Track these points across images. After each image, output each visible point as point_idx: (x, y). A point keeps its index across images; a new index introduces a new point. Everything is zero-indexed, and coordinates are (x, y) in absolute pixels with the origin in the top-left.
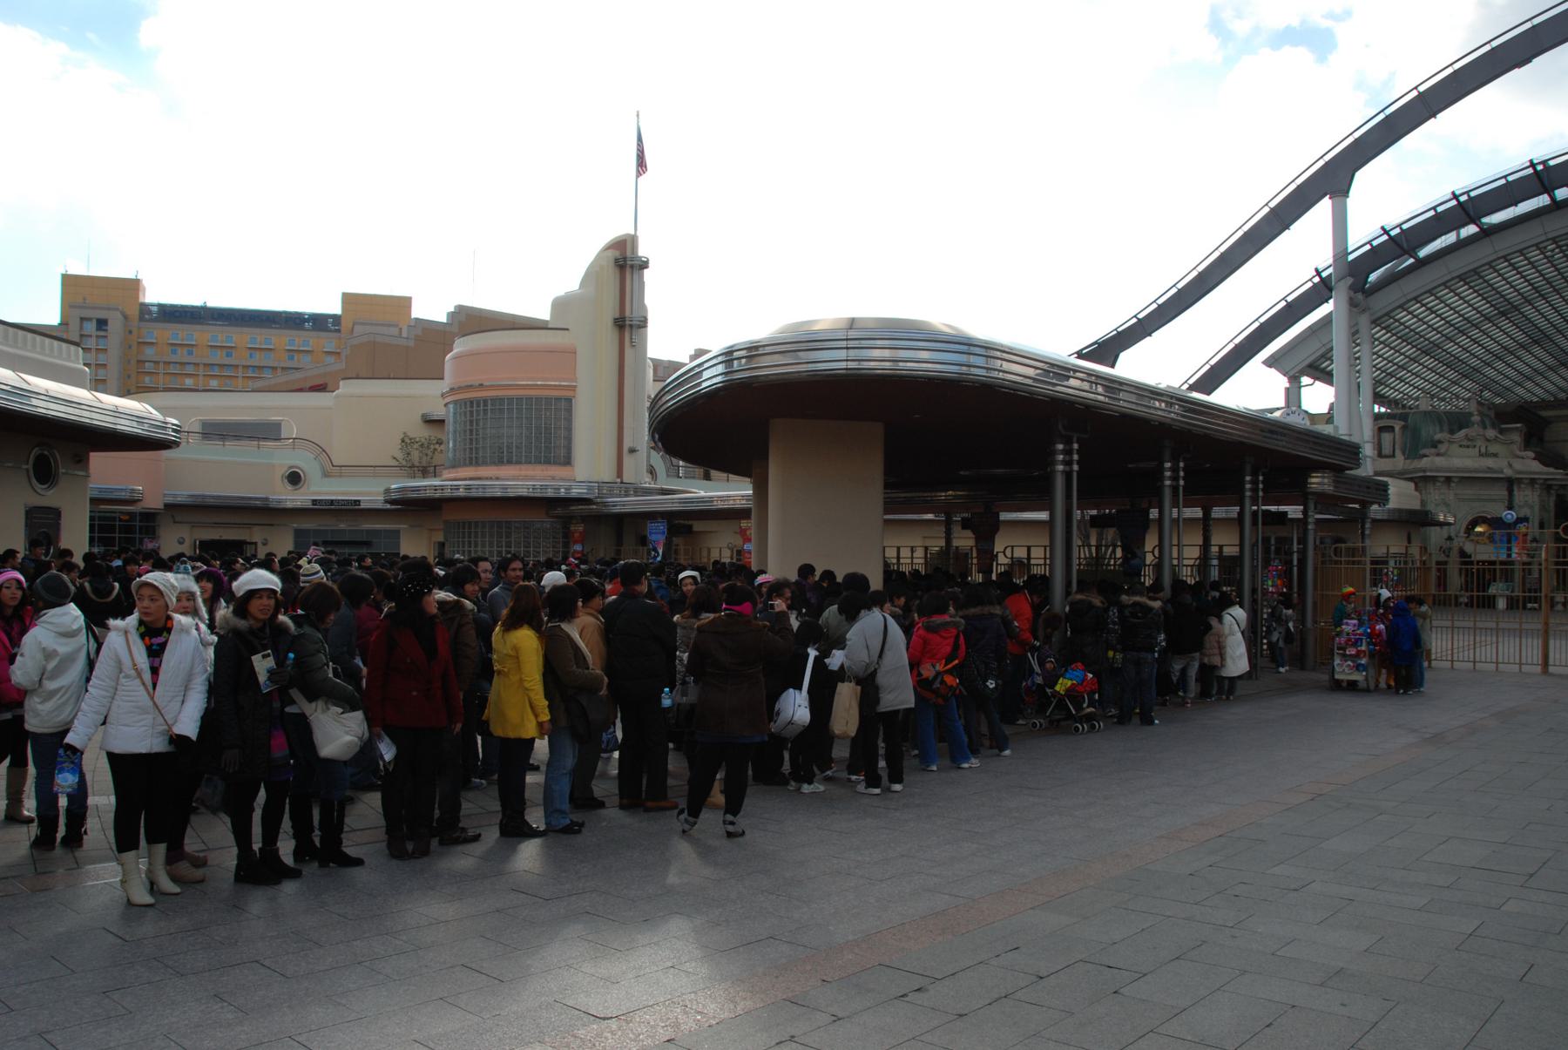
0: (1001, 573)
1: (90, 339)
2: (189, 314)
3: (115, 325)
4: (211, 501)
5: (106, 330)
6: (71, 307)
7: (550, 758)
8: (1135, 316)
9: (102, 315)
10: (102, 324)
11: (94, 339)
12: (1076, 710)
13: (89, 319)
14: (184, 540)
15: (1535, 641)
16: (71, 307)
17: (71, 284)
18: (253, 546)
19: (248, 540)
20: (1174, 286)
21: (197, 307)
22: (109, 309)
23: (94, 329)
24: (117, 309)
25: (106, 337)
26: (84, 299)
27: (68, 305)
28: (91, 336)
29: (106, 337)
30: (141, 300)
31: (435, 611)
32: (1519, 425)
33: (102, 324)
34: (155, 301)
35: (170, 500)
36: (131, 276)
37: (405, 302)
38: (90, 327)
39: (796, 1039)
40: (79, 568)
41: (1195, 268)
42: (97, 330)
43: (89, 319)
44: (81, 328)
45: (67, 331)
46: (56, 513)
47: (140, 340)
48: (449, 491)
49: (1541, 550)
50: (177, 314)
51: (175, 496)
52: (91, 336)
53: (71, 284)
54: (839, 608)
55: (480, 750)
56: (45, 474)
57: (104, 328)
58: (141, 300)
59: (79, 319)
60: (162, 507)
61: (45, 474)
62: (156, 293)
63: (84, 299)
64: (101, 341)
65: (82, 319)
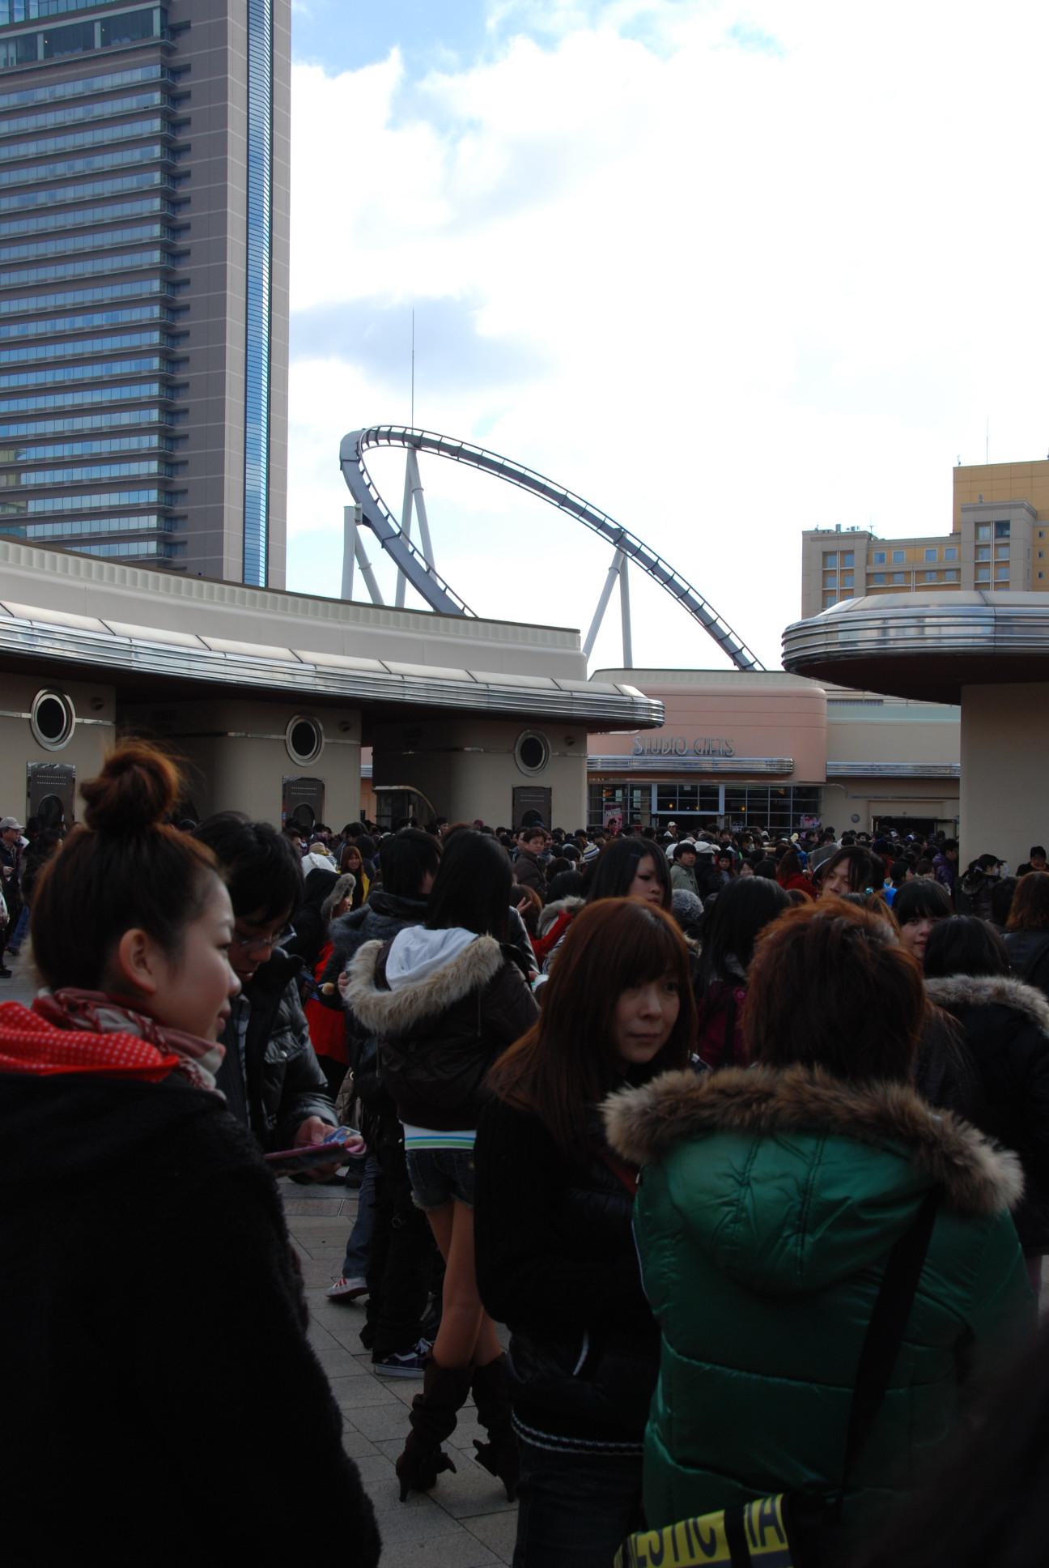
1: (986, 550)
3: (1020, 529)
4: (877, 774)
5: (1008, 536)
6: (964, 510)
7: (679, 1018)
8: (447, 587)
9: (1001, 516)
10: (1002, 527)
11: (992, 550)
12: (522, 898)
13: (987, 524)
14: (857, 815)
16: (964, 510)
17: (965, 477)
18: (952, 825)
19: (939, 818)
20: (606, 516)
22: (1010, 507)
24: (1021, 506)
25: (1007, 545)
26: (981, 497)
27: (962, 508)
28: (988, 546)
29: (1007, 545)
31: (895, 890)
33: (1002, 527)
35: (831, 773)
38: (987, 533)
40: (712, 854)
41: (588, 504)
42: (997, 537)
43: (987, 524)
45: (960, 543)
46: (317, 786)
51: (837, 767)
52: (988, 546)
53: (965, 477)
56: (532, 755)
57: (1007, 533)
59: (973, 524)
60: (824, 781)
61: (532, 755)
63: (981, 497)
64: (1002, 551)
65: (825, 554)
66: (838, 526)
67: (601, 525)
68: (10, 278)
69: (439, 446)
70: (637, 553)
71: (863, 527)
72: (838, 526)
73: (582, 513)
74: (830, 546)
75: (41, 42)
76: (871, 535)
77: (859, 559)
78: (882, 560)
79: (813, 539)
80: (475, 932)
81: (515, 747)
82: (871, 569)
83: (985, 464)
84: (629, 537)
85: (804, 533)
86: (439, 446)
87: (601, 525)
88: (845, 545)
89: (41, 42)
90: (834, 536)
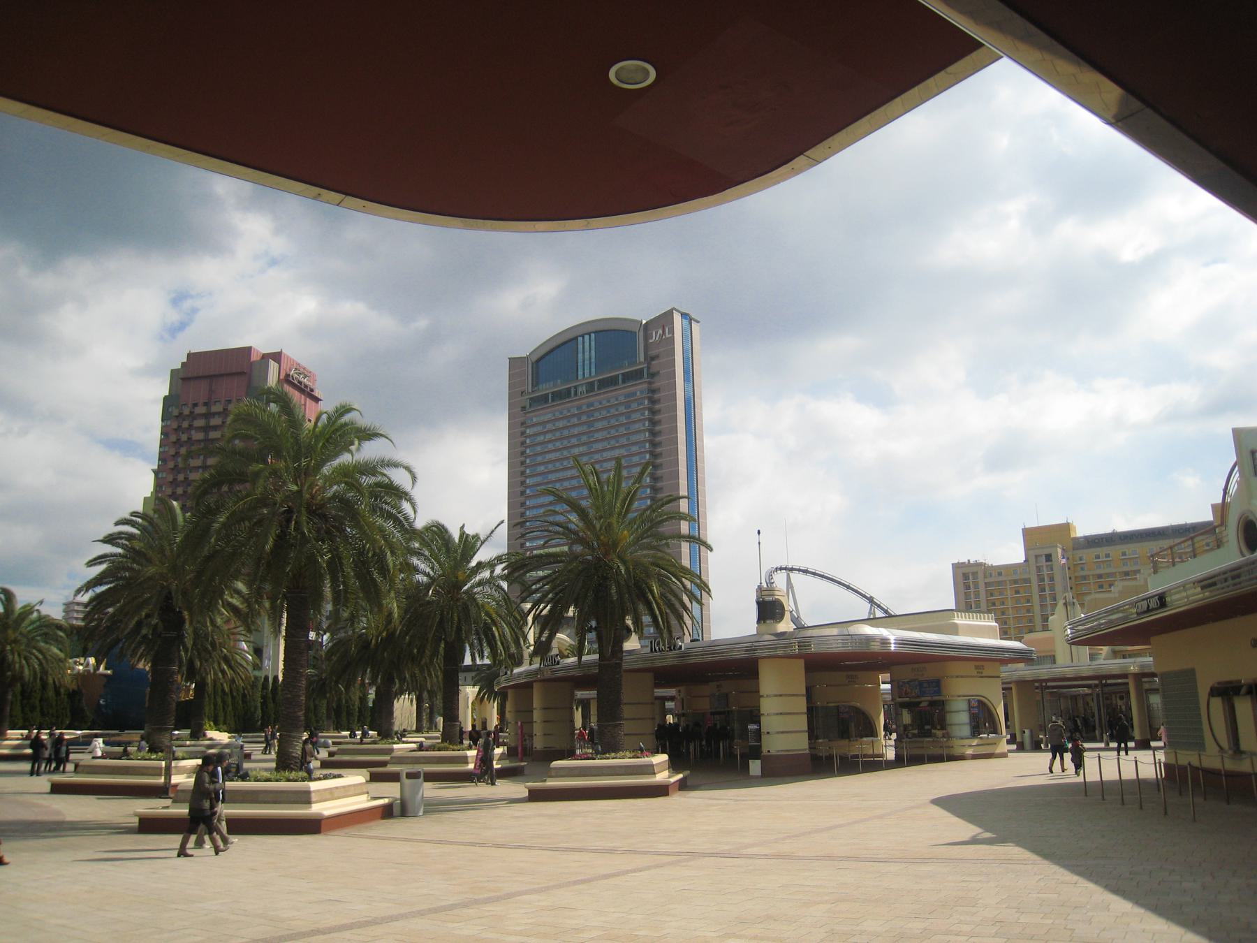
0: (674, 765)
2: (1104, 540)
9: (1047, 551)
15: (271, 383)
21: (1109, 534)
23: (1044, 561)
30: (1073, 535)
32: (721, 745)
34: (1082, 535)
36: (1062, 521)
37: (145, 499)
39: (1035, 937)
44: (1036, 562)
47: (1075, 563)
48: (878, 644)
49: (970, 595)
50: (1097, 541)
54: (191, 733)
55: (1254, 784)
58: (1073, 535)
59: (1034, 557)
60: (947, 600)
62: (1084, 528)
65: (1037, 557)
66: (969, 561)
67: (864, 596)
68: (891, 746)
69: (799, 570)
70: (879, 606)
71: (981, 561)
72: (969, 561)
73: (856, 591)
74: (966, 570)
75: (620, 377)
76: (985, 564)
77: (980, 575)
78: (991, 576)
79: (956, 567)
80: (980, 827)
81: (683, 630)
82: (987, 580)
83: (1037, 526)
84: (875, 600)
85: (953, 564)
86: (799, 570)
87: (864, 596)
88: (974, 569)
89: (620, 377)
90: (968, 565)
